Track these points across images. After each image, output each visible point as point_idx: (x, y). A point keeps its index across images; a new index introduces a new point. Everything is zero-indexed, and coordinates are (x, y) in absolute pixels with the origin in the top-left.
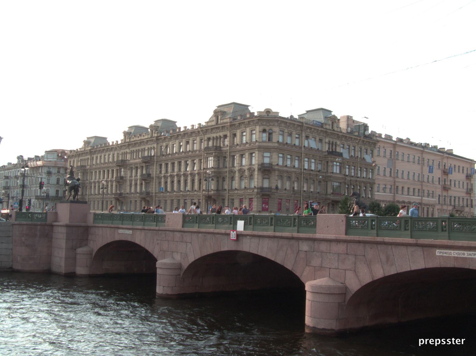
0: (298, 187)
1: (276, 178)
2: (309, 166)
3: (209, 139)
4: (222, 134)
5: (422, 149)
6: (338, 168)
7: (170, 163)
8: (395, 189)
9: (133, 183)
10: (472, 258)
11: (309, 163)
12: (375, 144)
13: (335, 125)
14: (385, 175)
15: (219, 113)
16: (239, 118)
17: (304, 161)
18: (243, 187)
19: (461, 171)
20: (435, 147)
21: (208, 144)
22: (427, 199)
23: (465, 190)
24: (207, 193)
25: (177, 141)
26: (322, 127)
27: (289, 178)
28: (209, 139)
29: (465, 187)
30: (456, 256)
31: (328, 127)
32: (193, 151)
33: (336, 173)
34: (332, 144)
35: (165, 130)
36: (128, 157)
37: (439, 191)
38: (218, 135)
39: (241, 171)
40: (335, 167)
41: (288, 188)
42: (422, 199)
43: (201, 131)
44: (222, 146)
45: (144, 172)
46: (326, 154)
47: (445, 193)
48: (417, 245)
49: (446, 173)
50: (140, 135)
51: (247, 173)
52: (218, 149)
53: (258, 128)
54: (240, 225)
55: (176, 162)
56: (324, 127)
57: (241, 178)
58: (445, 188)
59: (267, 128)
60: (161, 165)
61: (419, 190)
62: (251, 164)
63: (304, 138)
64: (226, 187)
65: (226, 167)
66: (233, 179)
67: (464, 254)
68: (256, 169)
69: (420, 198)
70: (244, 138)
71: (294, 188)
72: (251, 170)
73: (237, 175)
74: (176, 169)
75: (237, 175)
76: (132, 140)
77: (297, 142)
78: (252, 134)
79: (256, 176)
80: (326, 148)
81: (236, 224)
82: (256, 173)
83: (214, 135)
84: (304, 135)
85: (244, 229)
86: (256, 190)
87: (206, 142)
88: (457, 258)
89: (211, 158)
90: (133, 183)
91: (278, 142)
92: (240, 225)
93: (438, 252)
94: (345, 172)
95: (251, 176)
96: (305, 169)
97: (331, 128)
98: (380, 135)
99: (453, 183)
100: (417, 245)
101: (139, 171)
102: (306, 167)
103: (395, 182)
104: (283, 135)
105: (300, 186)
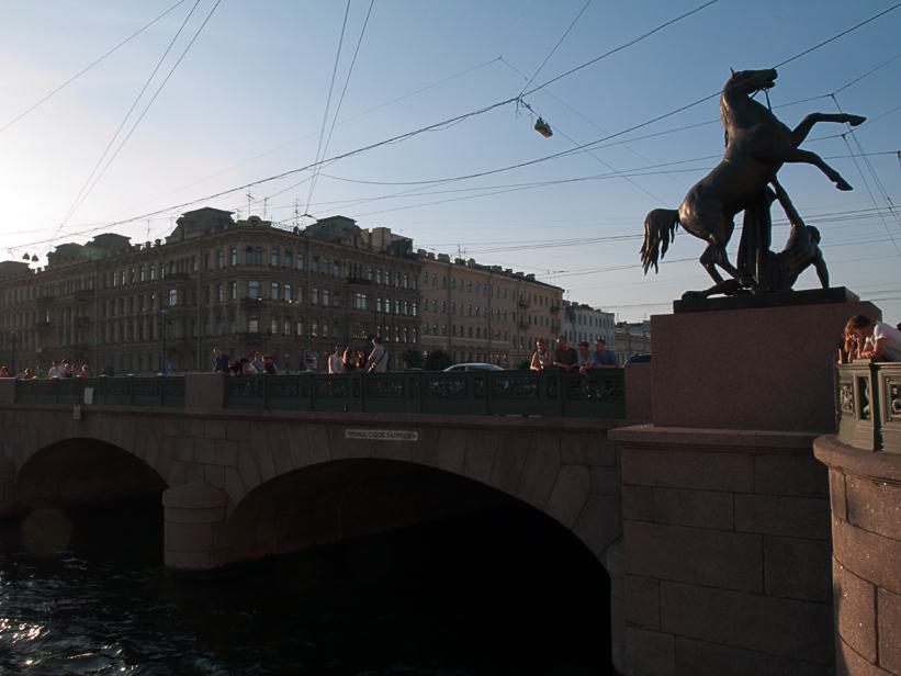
0: (303, 330)
1: (268, 318)
2: (383, 307)
3: (172, 263)
4: (188, 255)
5: (489, 274)
6: (364, 301)
7: (135, 298)
8: (451, 331)
9: (65, 332)
10: (394, 441)
11: (320, 295)
12: (420, 268)
13: (359, 240)
14: (435, 311)
15: (188, 222)
16: (213, 230)
17: (312, 293)
18: (220, 333)
19: (544, 302)
20: (509, 271)
21: (171, 270)
22: (469, 339)
23: (549, 329)
24: (487, 341)
25: (127, 267)
26: (339, 243)
27: (288, 318)
28: (172, 263)
29: (550, 324)
30: (373, 438)
31: (348, 243)
32: (149, 281)
33: (361, 309)
34: (355, 268)
35: (111, 246)
36: (57, 292)
37: (513, 330)
38: (184, 256)
39: (218, 309)
40: (358, 301)
41: (287, 333)
42: (450, 340)
43: (153, 253)
44: (190, 272)
45: (80, 315)
46: (346, 281)
47: (522, 334)
48: (316, 422)
49: (522, 305)
50: (73, 258)
51: (225, 311)
52: (184, 276)
53: (240, 246)
54: (89, 393)
55: (135, 298)
56: (342, 242)
57: (218, 319)
58: (522, 326)
59: (254, 245)
60: (105, 303)
61: (485, 330)
62: (231, 298)
63: (311, 259)
64: (196, 334)
65: (196, 305)
66: (206, 321)
67: (382, 435)
68: (238, 307)
69: (487, 341)
70: (221, 262)
71: (296, 332)
72: (231, 307)
73: (211, 315)
74: (135, 309)
75: (211, 315)
76: (62, 266)
77: (300, 265)
78: (232, 254)
79: (238, 317)
80: (346, 273)
81: (82, 394)
82: (238, 312)
83: (179, 257)
84: (310, 254)
85: (94, 399)
86: (238, 337)
87: (167, 268)
88: (375, 441)
89: (174, 291)
90: (65, 332)
91: (270, 265)
92: (89, 393)
93: (348, 433)
94: (376, 308)
95: (232, 317)
96: (313, 305)
97: (352, 244)
98: (431, 255)
99: (533, 320)
100: (316, 422)
101: (73, 313)
102: (315, 301)
103: (450, 320)
104: (278, 255)
105: (307, 329)
